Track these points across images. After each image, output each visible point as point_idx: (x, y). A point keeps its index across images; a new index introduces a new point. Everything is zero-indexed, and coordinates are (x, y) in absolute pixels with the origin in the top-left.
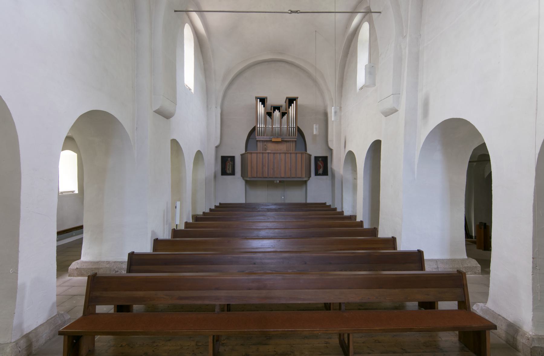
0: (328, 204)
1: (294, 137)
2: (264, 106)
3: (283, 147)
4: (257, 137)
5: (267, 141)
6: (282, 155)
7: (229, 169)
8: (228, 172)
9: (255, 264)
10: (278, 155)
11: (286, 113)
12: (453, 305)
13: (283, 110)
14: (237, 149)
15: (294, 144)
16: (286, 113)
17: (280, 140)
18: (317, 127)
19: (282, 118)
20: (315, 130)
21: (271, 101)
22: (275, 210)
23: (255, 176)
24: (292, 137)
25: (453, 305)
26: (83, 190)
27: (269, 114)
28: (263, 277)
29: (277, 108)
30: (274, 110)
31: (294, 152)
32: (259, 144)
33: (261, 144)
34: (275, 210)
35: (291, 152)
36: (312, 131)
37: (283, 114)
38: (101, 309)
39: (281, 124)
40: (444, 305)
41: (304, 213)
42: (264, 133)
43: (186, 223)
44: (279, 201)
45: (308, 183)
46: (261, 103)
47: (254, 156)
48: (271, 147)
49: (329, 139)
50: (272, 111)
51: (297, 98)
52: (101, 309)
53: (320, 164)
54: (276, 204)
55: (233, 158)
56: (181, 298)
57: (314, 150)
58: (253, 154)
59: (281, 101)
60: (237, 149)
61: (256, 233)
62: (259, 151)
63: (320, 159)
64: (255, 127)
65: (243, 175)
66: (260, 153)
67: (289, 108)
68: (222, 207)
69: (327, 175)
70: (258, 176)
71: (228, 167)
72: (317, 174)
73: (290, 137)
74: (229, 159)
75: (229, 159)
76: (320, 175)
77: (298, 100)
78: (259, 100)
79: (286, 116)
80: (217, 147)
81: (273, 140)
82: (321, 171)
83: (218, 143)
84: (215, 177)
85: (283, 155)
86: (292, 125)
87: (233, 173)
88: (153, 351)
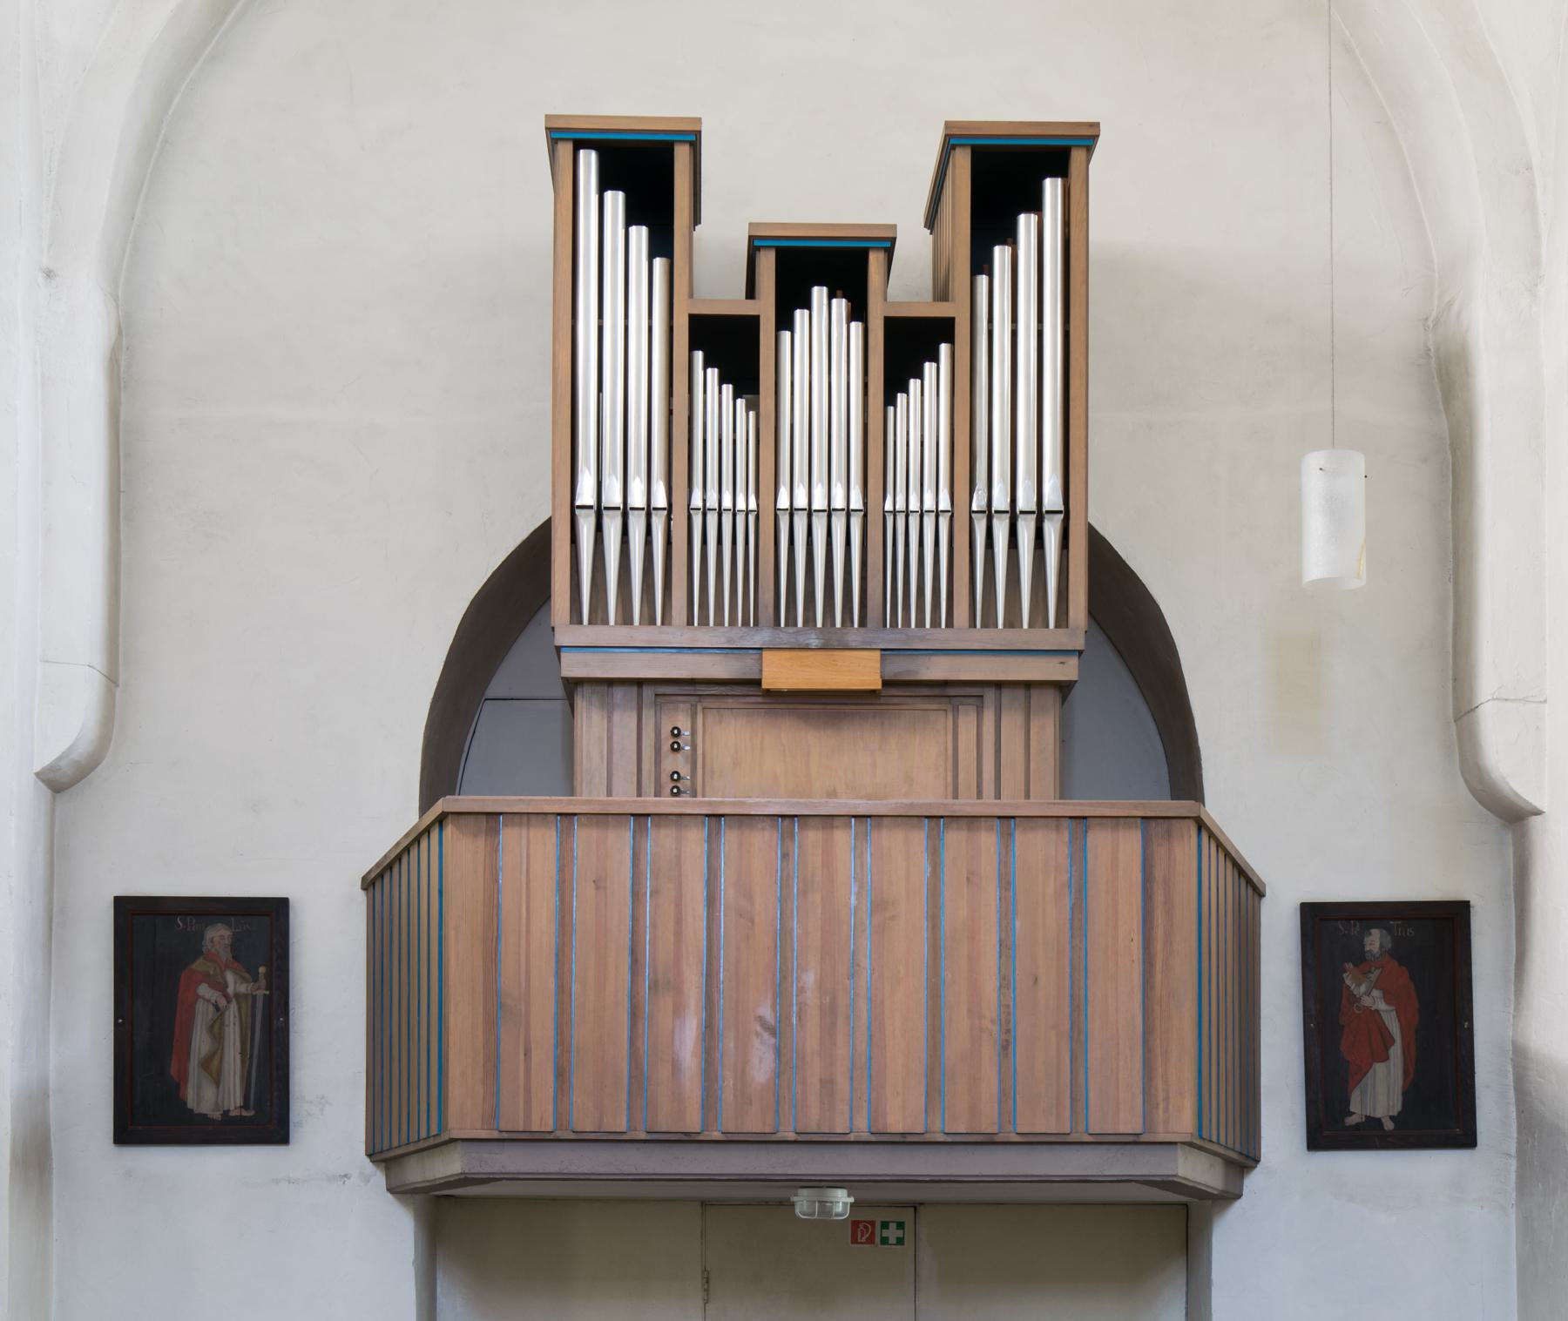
1: (1050, 636)
2: (661, 245)
3: (904, 764)
4: (566, 635)
6: (893, 840)
8: (203, 1097)
10: (843, 838)
11: (943, 329)
13: (905, 284)
14: (306, 803)
15: (1045, 729)
16: (943, 329)
17: (859, 670)
18: (1353, 484)
19: (895, 383)
20: (1315, 525)
21: (741, 199)
23: (542, 1120)
24: (1025, 635)
27: (730, 347)
28: (811, 998)
29: (820, 266)
30: (791, 299)
31: (1044, 800)
32: (590, 722)
33: (625, 721)
35: (1012, 803)
36: (1263, 567)
37: (908, 347)
39: (875, 461)
42: (672, 570)
45: (1232, 1239)
46: (616, 200)
47: (530, 854)
48: (749, 762)
49: (1489, 680)
50: (765, 307)
51: (1087, 138)
53: (1376, 1001)
55: (263, 926)
57: (1314, 821)
58: (509, 836)
59: (886, 187)
60: (306, 803)
62: (591, 795)
63: (1375, 941)
64: (539, 542)
65: (386, 1151)
66: (602, 818)
67: (981, 264)
69: (1461, 1134)
70: (585, 1122)
71: (201, 1043)
72: (1330, 1127)
73: (1000, 636)
74: (218, 936)
75: (218, 936)
76: (1369, 1137)
77: (1103, 171)
78: (589, 161)
79: (935, 375)
80: (61, 784)
81: (780, 673)
82: (1381, 1091)
83: (68, 727)
84: (36, 1157)
85: (904, 852)
86: (1021, 472)
87: (265, 1119)
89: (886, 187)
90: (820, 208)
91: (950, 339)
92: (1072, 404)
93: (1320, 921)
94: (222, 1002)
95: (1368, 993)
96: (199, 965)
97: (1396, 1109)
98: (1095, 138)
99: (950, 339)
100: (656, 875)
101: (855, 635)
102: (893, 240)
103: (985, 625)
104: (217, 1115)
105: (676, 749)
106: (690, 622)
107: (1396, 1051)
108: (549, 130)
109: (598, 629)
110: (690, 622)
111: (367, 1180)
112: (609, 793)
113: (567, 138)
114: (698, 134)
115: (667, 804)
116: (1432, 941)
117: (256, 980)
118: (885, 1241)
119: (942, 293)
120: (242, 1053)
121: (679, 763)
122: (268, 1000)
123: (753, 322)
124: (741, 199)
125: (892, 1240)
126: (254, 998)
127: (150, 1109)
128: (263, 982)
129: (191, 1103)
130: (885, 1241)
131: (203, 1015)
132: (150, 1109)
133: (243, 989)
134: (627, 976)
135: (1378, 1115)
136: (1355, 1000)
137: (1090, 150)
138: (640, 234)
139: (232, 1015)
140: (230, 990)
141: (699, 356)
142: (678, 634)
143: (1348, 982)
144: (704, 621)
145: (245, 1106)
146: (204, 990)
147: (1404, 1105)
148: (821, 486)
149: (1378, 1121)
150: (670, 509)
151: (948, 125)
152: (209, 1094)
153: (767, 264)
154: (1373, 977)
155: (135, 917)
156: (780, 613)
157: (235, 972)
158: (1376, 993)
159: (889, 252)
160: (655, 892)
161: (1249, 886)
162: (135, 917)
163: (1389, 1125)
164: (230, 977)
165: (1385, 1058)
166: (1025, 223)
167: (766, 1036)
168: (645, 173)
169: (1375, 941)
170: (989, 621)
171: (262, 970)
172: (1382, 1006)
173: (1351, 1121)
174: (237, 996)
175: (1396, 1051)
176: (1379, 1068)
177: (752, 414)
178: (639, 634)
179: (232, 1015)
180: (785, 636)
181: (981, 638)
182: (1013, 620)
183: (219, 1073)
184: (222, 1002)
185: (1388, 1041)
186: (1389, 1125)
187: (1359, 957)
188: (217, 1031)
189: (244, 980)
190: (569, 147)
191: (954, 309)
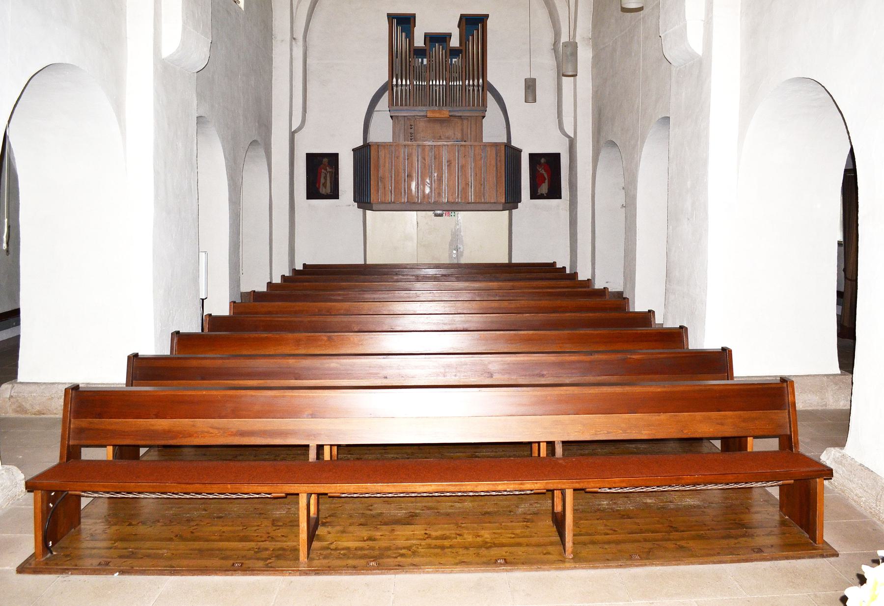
0: (559, 266)
5: (495, 545)
7: (325, 185)
8: (323, 191)
9: (386, 378)
12: (772, 445)
22: (435, 278)
25: (772, 445)
26: (570, 170)
34: (435, 278)
38: (89, 454)
40: (755, 445)
41: (501, 284)
43: (283, 277)
44: (445, 260)
51: (487, 16)
52: (89, 454)
54: (437, 266)
55: (334, 158)
56: (242, 434)
59: (450, 26)
61: (389, 322)
63: (543, 160)
68: (312, 272)
69: (560, 198)
71: (322, 180)
72: (534, 195)
75: (325, 160)
76: (541, 197)
77: (489, 22)
81: (429, 115)
82: (544, 189)
87: (334, 194)
88: (192, 533)
89: (450, 26)
93: (532, 156)
97: (547, 191)
113: (391, 17)
116: (553, 160)
127: (313, 193)
131: (323, 175)
132: (313, 193)
134: (562, 388)
142: (411, 108)
153: (428, 40)
161: (519, 152)
168: (403, 22)
169: (543, 160)
170: (469, 105)
180: (432, 108)
182: (473, 105)
185: (545, 179)
187: (540, 164)
188: (325, 178)
191: (463, 48)
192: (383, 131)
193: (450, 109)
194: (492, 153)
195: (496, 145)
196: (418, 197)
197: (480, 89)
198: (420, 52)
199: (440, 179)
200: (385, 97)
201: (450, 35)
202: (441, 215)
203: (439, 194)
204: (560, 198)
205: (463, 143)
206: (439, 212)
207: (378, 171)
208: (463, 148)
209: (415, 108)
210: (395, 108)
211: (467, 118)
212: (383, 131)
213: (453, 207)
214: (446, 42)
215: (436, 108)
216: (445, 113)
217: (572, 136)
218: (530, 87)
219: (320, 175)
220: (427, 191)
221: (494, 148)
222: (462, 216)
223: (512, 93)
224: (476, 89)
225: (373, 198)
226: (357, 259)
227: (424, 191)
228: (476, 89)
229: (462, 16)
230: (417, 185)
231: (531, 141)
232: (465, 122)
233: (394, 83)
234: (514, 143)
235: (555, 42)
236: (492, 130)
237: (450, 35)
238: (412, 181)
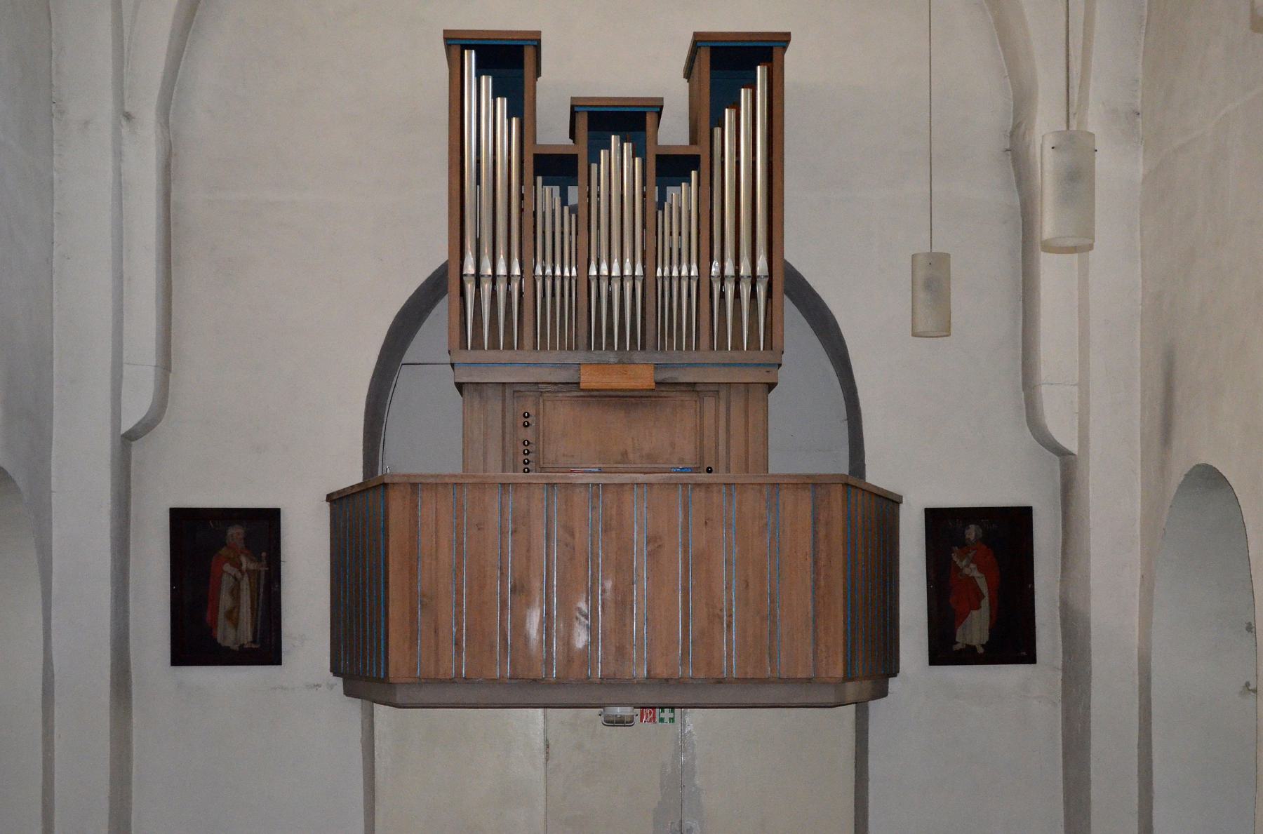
2: (515, 110)
7: (233, 617)
8: (226, 636)
13: (673, 132)
30: (598, 144)
37: (673, 168)
50: (582, 151)
51: (783, 40)
53: (973, 571)
55: (263, 526)
63: (972, 532)
69: (1031, 659)
71: (225, 601)
72: (944, 650)
73: (729, 354)
74: (235, 533)
75: (235, 533)
76: (968, 657)
77: (792, 59)
78: (471, 58)
81: (590, 379)
87: (266, 649)
90: (617, 83)
91: (697, 168)
92: (774, 223)
93: (937, 519)
94: (239, 575)
95: (967, 566)
96: (224, 551)
98: (788, 41)
99: (697, 168)
100: (514, 521)
101: (638, 356)
102: (661, 107)
103: (719, 348)
104: (236, 647)
105: (526, 425)
106: (535, 347)
107: (985, 603)
108: (446, 39)
109: (478, 353)
110: (535, 347)
111: (331, 687)
112: (485, 471)
113: (456, 43)
114: (539, 41)
115: (520, 477)
116: (1008, 531)
117: (260, 560)
118: (662, 720)
119: (694, 139)
120: (252, 608)
121: (529, 434)
122: (267, 574)
123: (574, 158)
124: (558, 86)
125: (667, 720)
126: (259, 572)
127: (193, 644)
128: (264, 562)
129: (219, 640)
130: (662, 720)
131: (227, 583)
132: (193, 644)
133: (252, 566)
135: (975, 643)
136: (958, 570)
137: (785, 48)
138: (502, 103)
139: (245, 585)
140: (244, 567)
141: (539, 179)
142: (527, 355)
143: (955, 559)
144: (544, 348)
145: (254, 642)
146: (227, 567)
147: (990, 636)
148: (617, 268)
149: (974, 648)
150: (521, 276)
151: (696, 34)
152: (231, 633)
153: (582, 122)
154: (971, 555)
155: (187, 525)
156: (592, 341)
157: (246, 555)
158: (972, 566)
159: (659, 114)
160: (514, 532)
162: (187, 525)
163: (981, 650)
164: (243, 559)
165: (978, 607)
166: (744, 94)
167: (583, 619)
168: (506, 61)
169: (972, 532)
170: (722, 346)
171: (264, 554)
172: (976, 574)
173: (957, 647)
174: (248, 570)
175: (985, 603)
176: (974, 613)
177: (573, 216)
178: (505, 356)
179: (245, 585)
180: (595, 356)
181: (717, 356)
182: (737, 346)
183: (238, 618)
184: (239, 575)
185: (980, 596)
186: (981, 650)
187: (963, 544)
188: (235, 593)
189: (252, 560)
190: (458, 49)
191: (701, 150)
192: (432, 436)
193: (659, 358)
194: (799, 508)
195: (815, 485)
196: (548, 662)
197: (761, 290)
198: (556, 168)
199: (623, 603)
200: (441, 315)
201: (657, 108)
202: (621, 722)
203: (621, 652)
204: (1031, 659)
205: (703, 477)
206: (618, 711)
207: (413, 572)
208: (699, 495)
209: (544, 357)
210: (470, 355)
211: (716, 389)
212: (432, 436)
213: (663, 696)
214: (643, 128)
215: (612, 358)
216: (641, 376)
217: (1073, 447)
218: (933, 279)
219: (217, 581)
220: (581, 639)
221: (806, 497)
222: (694, 719)
223: (869, 310)
224: (745, 290)
225: (398, 661)
226: (549, 710)
227: (568, 641)
228: (745, 290)
229: (699, 41)
230: (547, 619)
231: (929, 462)
232: (709, 403)
233: (470, 269)
234: (876, 476)
235: (1017, 126)
236: (798, 437)
237: (657, 108)
238: (529, 605)
